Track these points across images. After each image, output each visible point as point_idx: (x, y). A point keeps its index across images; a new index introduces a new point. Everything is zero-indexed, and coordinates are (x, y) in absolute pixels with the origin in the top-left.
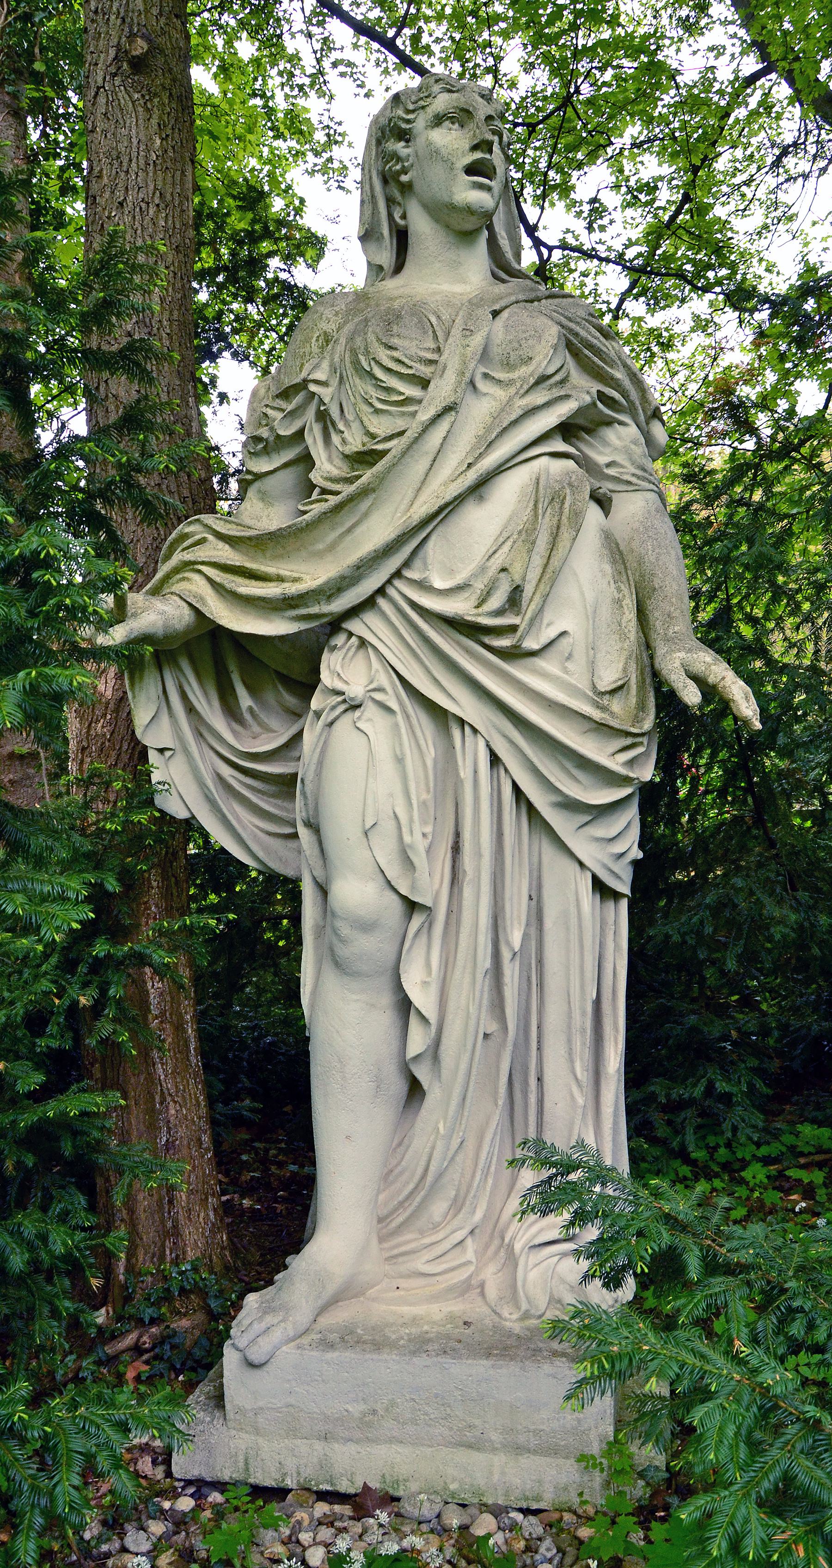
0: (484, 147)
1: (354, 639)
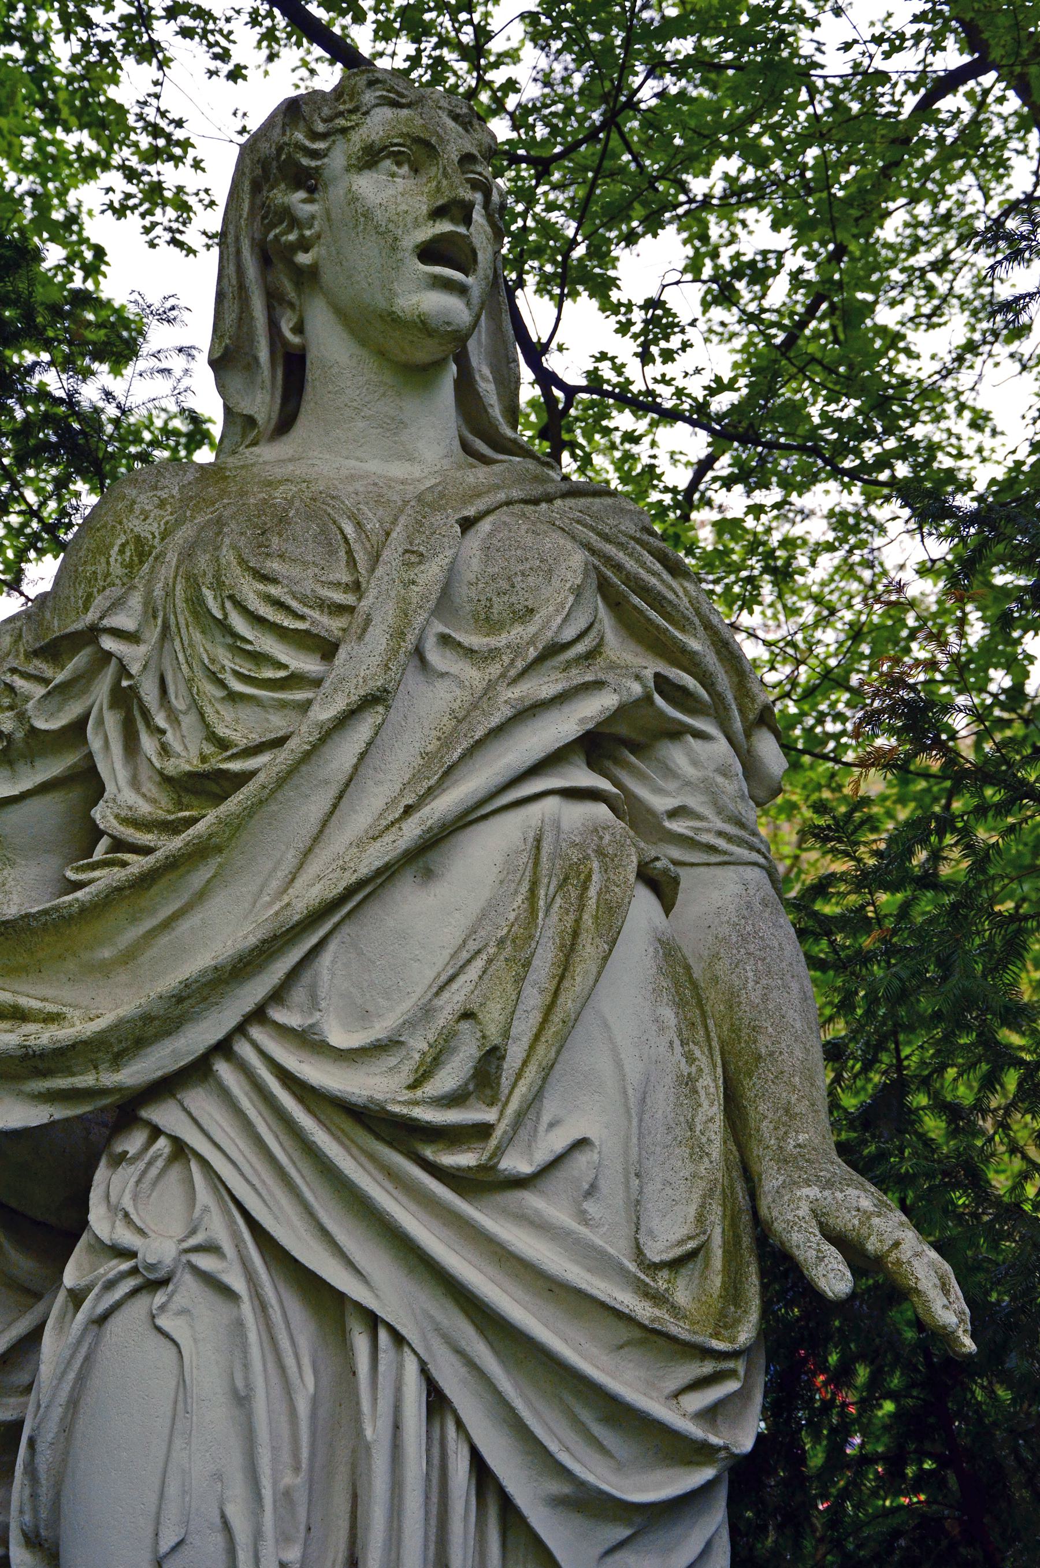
0: (455, 211)
1: (162, 1143)
